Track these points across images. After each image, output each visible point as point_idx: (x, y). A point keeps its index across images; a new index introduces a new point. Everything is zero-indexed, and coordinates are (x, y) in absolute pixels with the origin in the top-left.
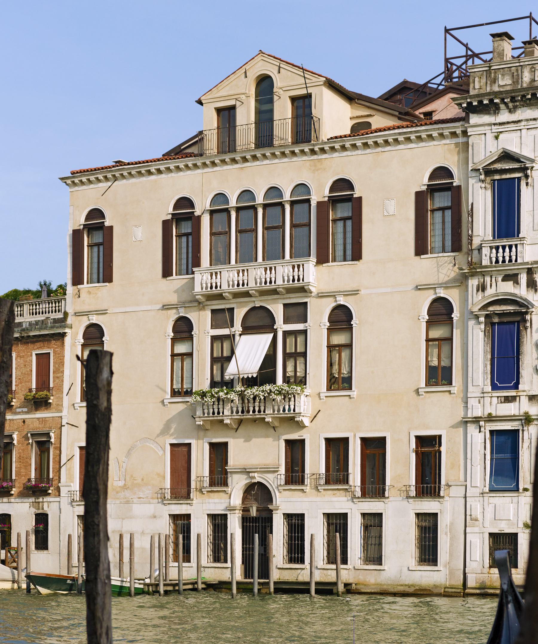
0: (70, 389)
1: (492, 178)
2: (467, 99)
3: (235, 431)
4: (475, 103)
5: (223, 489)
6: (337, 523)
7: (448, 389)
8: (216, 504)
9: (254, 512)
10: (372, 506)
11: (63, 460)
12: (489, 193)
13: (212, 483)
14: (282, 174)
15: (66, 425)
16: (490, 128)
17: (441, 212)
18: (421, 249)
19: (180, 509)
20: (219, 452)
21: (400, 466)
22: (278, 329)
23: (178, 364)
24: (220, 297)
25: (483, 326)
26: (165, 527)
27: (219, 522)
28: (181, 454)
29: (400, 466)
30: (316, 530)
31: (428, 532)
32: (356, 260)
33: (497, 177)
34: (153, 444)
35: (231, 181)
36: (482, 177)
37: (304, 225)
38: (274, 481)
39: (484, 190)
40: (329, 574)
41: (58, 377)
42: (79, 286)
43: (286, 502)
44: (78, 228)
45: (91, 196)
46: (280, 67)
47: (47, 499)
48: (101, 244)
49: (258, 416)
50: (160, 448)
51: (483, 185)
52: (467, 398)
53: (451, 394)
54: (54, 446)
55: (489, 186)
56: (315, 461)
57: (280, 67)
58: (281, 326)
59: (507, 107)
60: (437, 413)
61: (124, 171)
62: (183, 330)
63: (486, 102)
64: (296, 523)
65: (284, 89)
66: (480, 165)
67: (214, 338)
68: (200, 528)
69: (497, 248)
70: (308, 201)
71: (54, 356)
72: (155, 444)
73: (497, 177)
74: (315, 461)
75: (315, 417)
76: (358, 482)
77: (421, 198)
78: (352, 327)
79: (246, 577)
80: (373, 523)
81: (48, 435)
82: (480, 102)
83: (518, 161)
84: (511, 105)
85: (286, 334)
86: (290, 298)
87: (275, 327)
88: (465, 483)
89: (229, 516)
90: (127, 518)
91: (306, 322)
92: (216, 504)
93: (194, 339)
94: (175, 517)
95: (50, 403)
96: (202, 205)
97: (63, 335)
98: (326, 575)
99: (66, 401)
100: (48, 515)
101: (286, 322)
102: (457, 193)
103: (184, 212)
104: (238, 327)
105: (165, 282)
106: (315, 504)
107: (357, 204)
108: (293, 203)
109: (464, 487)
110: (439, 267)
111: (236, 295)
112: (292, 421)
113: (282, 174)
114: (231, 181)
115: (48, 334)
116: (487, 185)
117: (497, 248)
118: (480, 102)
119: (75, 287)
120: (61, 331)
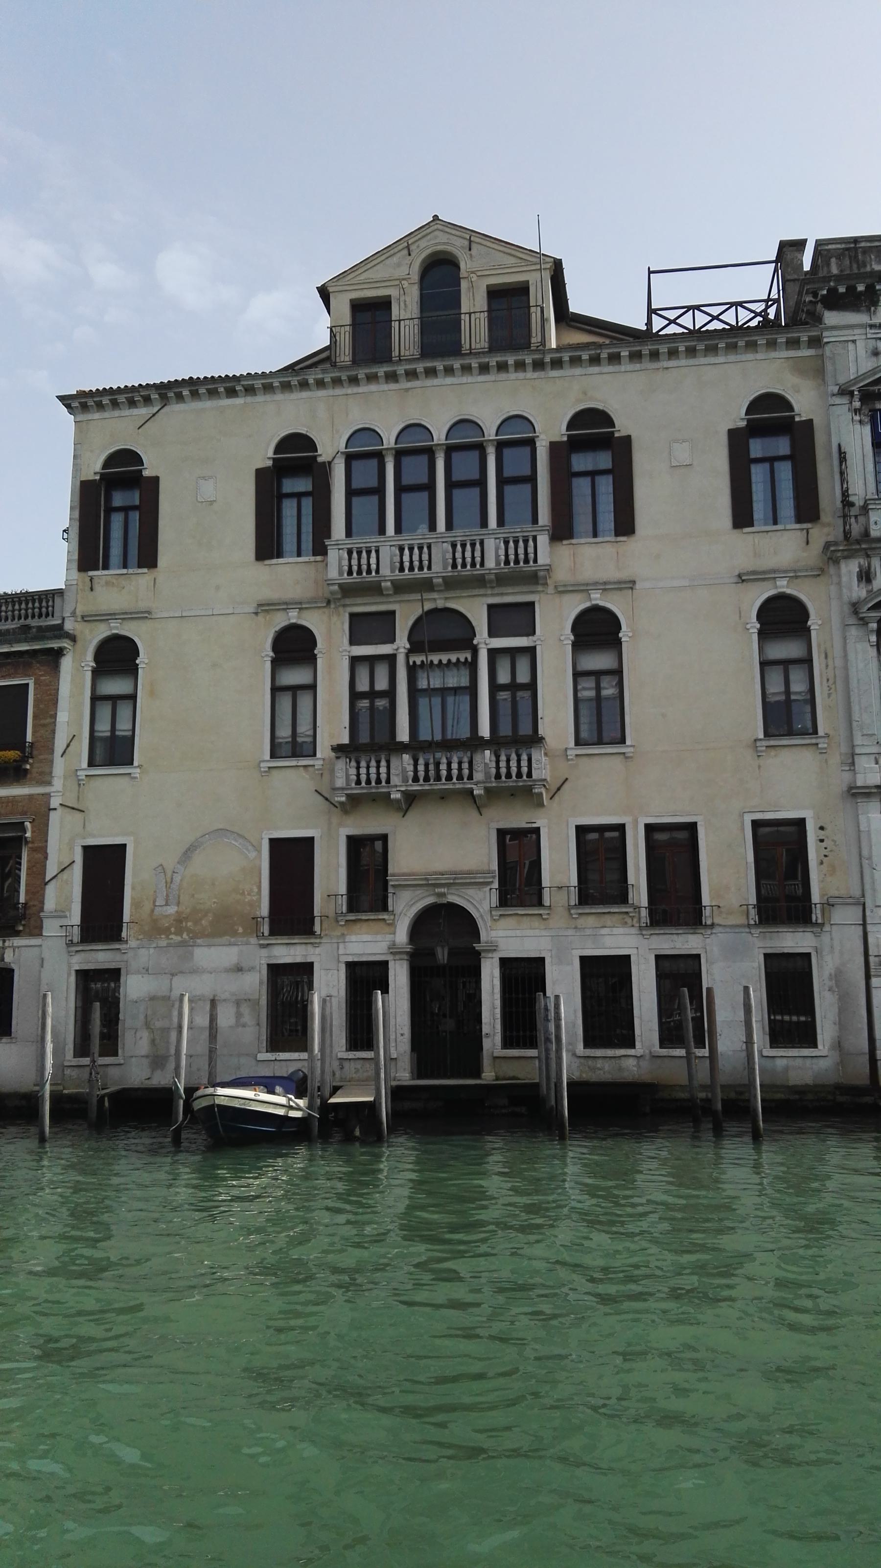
0: (68, 746)
1: (871, 406)
2: (829, 281)
3: (402, 814)
4: (842, 290)
5: (381, 917)
7: (814, 741)
8: (368, 942)
9: (442, 955)
10: (680, 942)
11: (51, 870)
12: (867, 430)
13: (354, 905)
14: (486, 400)
15: (60, 810)
16: (863, 331)
17: (767, 465)
18: (742, 517)
19: (289, 952)
21: (727, 874)
22: (480, 646)
23: (285, 702)
24: (374, 589)
25: (874, 638)
26: (254, 983)
27: (366, 979)
28: (291, 861)
29: (727, 874)
30: (564, 989)
31: (789, 988)
32: (624, 535)
34: (236, 841)
35: (385, 410)
36: (857, 404)
37: (788, 280)
38: (481, 902)
39: (858, 426)
40: (599, 1066)
41: (44, 725)
42: (91, 573)
43: (507, 936)
44: (91, 478)
45: (118, 431)
46: (470, 241)
47: (17, 941)
48: (134, 508)
49: (458, 786)
50: (250, 848)
51: (857, 418)
52: (853, 755)
53: (818, 748)
54: (30, 845)
55: (866, 419)
56: (559, 864)
57: (470, 241)
58: (484, 641)
61: (183, 387)
62: (294, 646)
63: (861, 288)
64: (525, 979)
65: (479, 273)
66: (854, 384)
67: (355, 661)
68: (328, 990)
70: (531, 443)
71: (35, 689)
72: (241, 840)
74: (559, 864)
75: (559, 789)
76: (644, 901)
77: (738, 441)
78: (621, 643)
79: (420, 1076)
81: (21, 826)
82: (851, 289)
85: (493, 653)
86: (502, 594)
87: (475, 642)
88: (862, 900)
89: (391, 965)
90: (181, 972)
91: (534, 633)
92: (368, 942)
93: (319, 661)
94: (276, 971)
95: (26, 770)
96: (330, 446)
97: (59, 653)
98: (593, 1069)
99: (59, 767)
100: (13, 970)
101: (492, 634)
102: (802, 436)
103: (295, 457)
104: (402, 643)
105: (744, 540)
106: (558, 941)
107: (622, 449)
108: (501, 446)
109: (861, 908)
110: (782, 547)
111: (400, 588)
112: (526, 793)
113: (486, 400)
114: (385, 410)
115: (27, 651)
116: (863, 418)
118: (851, 289)
119: (83, 574)
120: (54, 645)
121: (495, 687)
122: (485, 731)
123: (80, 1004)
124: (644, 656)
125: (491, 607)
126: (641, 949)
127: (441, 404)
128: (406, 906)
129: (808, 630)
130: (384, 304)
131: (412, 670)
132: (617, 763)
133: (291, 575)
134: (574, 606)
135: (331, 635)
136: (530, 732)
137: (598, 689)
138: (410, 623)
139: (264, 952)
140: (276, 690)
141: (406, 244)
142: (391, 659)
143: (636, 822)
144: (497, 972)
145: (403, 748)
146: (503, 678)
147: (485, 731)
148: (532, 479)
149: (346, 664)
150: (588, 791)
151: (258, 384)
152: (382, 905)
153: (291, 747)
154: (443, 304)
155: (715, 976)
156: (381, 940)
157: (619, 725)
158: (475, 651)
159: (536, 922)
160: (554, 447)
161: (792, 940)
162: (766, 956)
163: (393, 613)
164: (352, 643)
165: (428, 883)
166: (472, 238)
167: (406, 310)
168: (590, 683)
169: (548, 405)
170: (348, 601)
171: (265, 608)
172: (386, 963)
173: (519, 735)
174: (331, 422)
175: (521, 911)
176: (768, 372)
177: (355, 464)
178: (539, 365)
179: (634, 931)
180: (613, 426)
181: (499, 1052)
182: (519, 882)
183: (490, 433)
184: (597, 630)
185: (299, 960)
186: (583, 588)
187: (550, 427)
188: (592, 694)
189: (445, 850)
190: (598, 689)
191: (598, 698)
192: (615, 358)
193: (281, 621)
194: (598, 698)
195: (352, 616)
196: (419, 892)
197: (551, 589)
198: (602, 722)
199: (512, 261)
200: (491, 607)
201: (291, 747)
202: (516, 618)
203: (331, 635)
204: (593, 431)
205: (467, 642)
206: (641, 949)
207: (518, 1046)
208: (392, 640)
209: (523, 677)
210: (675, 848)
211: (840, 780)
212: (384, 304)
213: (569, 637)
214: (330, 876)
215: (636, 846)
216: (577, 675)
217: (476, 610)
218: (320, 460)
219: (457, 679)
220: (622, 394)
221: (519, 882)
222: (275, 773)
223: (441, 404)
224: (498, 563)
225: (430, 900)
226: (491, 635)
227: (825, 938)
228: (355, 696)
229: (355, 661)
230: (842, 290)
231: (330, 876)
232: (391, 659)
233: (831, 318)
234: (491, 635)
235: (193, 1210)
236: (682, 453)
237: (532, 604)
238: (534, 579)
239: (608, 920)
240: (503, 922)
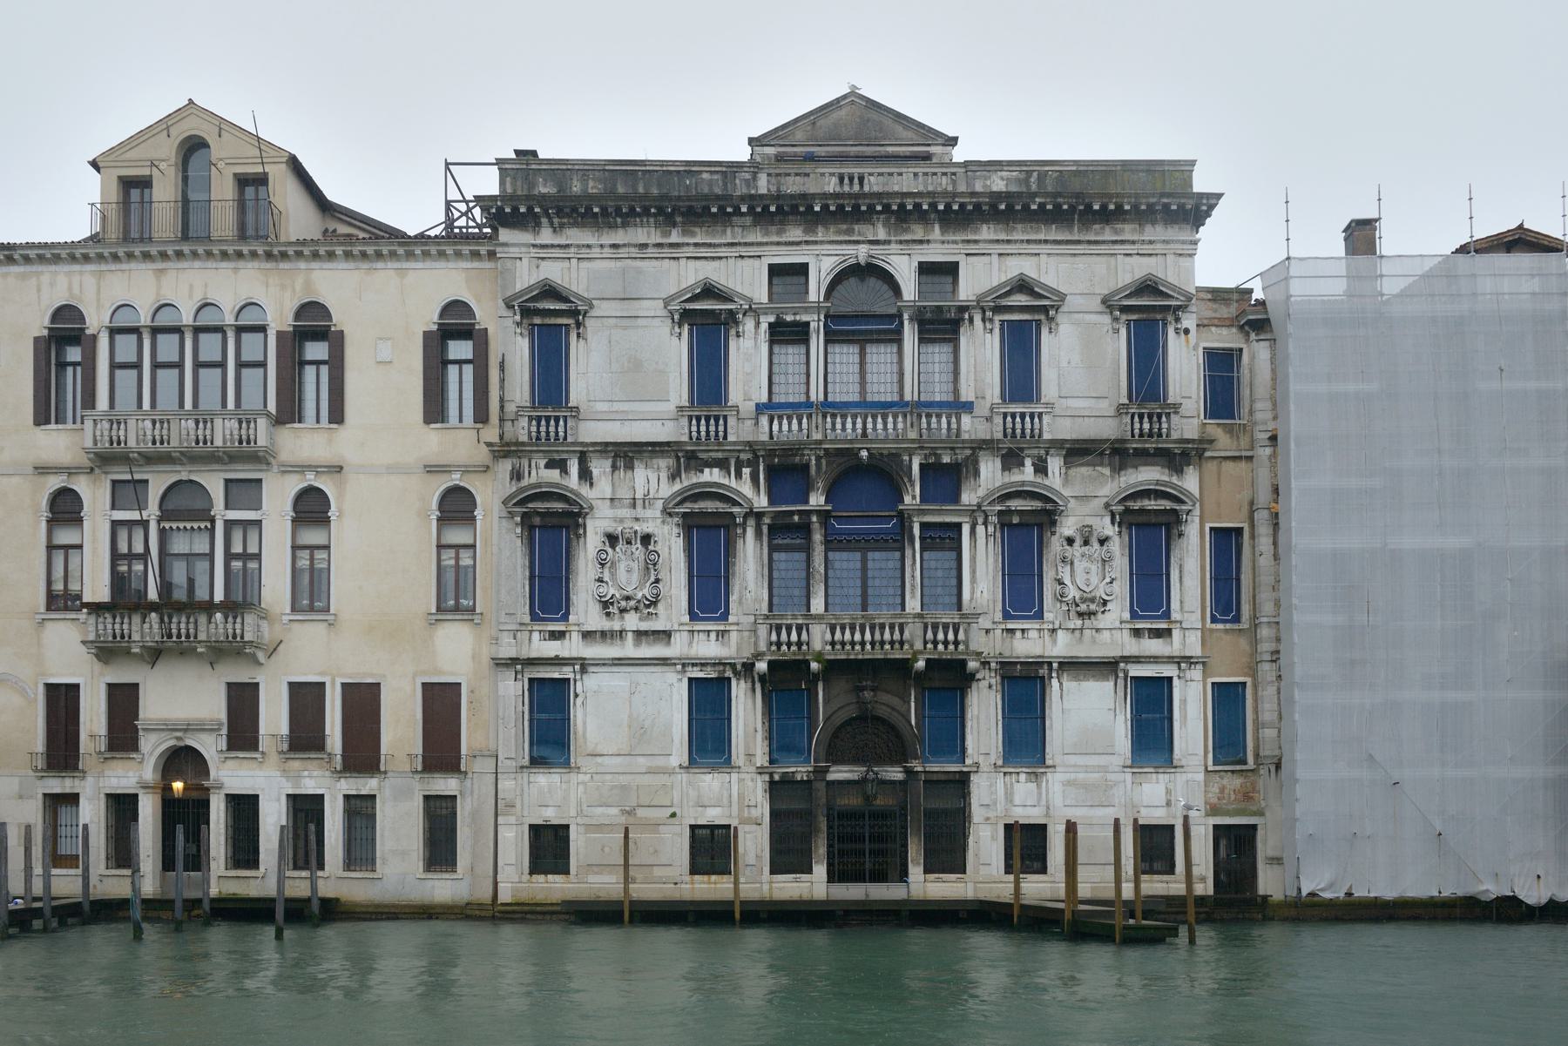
6: (306, 810)
18: (435, 410)
20: (123, 701)
21: (401, 729)
24: (124, 459)
25: (519, 530)
27: (122, 807)
28: (62, 700)
29: (401, 729)
30: (273, 818)
33: (537, 321)
35: (138, 289)
36: (518, 318)
38: (210, 746)
43: (231, 775)
56: (274, 717)
59: (552, 224)
60: (456, 653)
64: (244, 808)
67: (116, 525)
68: (92, 813)
69: (698, 419)
70: (262, 329)
73: (537, 321)
74: (274, 717)
80: (360, 811)
82: (515, 209)
83: (566, 300)
84: (556, 220)
85: (229, 524)
96: (96, 320)
104: (152, 511)
106: (270, 782)
107: (337, 342)
113: (229, 287)
114: (138, 289)
117: (698, 419)
118: (515, 209)
121: (229, 556)
122: (219, 596)
123: (112, 822)
124: (350, 538)
125: (227, 481)
126: (334, 791)
127: (190, 287)
128: (152, 747)
129: (473, 519)
130: (145, 183)
131: (162, 532)
132: (321, 628)
133: (61, 444)
134: (294, 485)
135: (95, 496)
136: (207, 598)
137: (457, 559)
138: (161, 492)
139: (39, 783)
140: (51, 548)
141: (165, 125)
142: (144, 524)
143: (333, 684)
144: (222, 806)
145: (153, 607)
146: (237, 548)
147: (219, 596)
148: (262, 365)
149: (107, 526)
150: (311, 654)
151: (64, 253)
152: (134, 747)
153: (61, 601)
154: (194, 189)
155: (385, 814)
156: (135, 774)
157: (954, 582)
158: (213, 521)
159: (254, 764)
160: (280, 335)
161: (445, 785)
162: (427, 798)
163: (146, 481)
164: (113, 507)
165: (168, 727)
166: (222, 125)
167: (165, 191)
168: (305, 554)
169: (275, 296)
170: (108, 469)
171: (432, 469)
172: (136, 796)
173: (240, 603)
174: (102, 296)
175: (241, 754)
176: (447, 281)
177: (118, 338)
178: (269, 256)
179: (328, 774)
180: (330, 319)
181: (222, 872)
182: (242, 732)
183: (229, 319)
184: (311, 508)
185: (68, 791)
186: (301, 469)
187: (279, 316)
188: (452, 562)
189: (182, 699)
190: (457, 559)
191: (457, 565)
192: (331, 255)
193: (55, 482)
194: (457, 565)
195: (114, 482)
196: (163, 734)
197: (275, 469)
198: (311, 592)
199: (123, 157)
200: (227, 481)
201: (61, 601)
202: (244, 491)
203: (95, 496)
204: (313, 324)
205: (207, 516)
206: (334, 791)
207: (858, 877)
208: (141, 507)
209: (253, 549)
210: (363, 702)
211: (486, 652)
212: (145, 183)
213: (290, 513)
214: (93, 717)
215: (333, 701)
216: (295, 548)
217: (214, 483)
218: (88, 332)
219: (201, 546)
220: (341, 288)
221: (242, 732)
222: (49, 625)
223: (190, 287)
224: (224, 441)
225: (172, 743)
226: (227, 507)
227: (468, 783)
228: (115, 556)
229: (116, 525)
230: (508, 210)
231: (93, 717)
232: (144, 524)
233: (505, 235)
234: (227, 507)
235: (46, 999)
236: (385, 352)
237: (260, 481)
238: (259, 458)
239: (308, 764)
240: (230, 763)
